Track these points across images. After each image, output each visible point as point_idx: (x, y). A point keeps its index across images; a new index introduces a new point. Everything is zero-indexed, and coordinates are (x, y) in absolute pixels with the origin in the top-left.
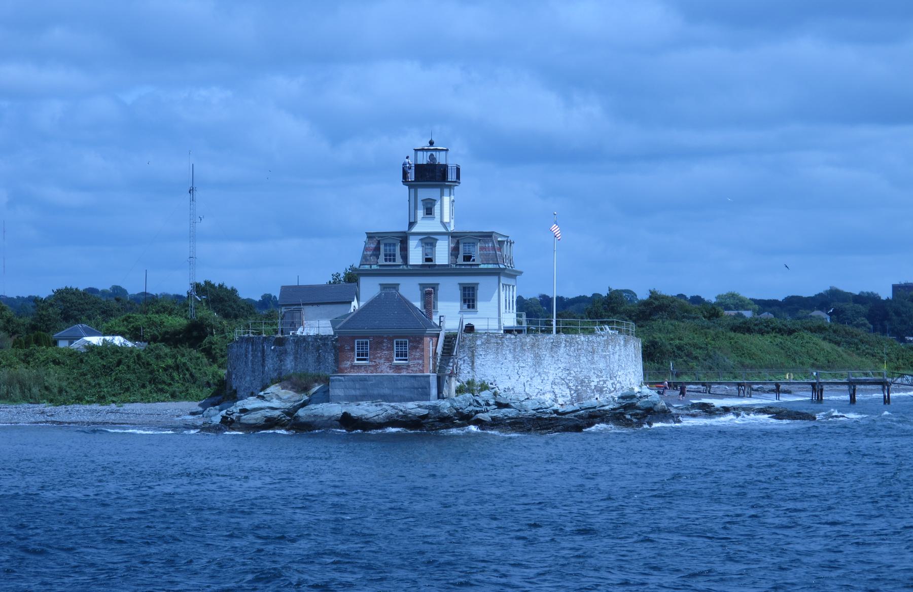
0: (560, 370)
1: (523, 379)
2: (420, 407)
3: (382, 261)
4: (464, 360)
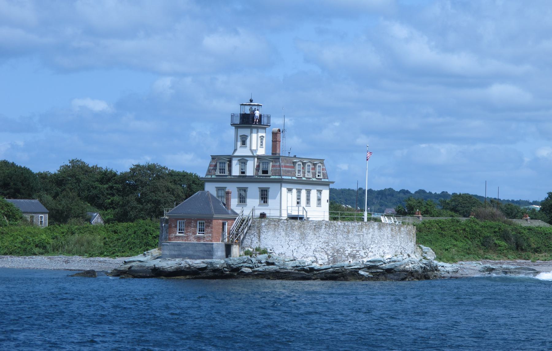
0: (321, 243)
1: (291, 248)
2: (203, 262)
3: (218, 173)
4: (254, 235)
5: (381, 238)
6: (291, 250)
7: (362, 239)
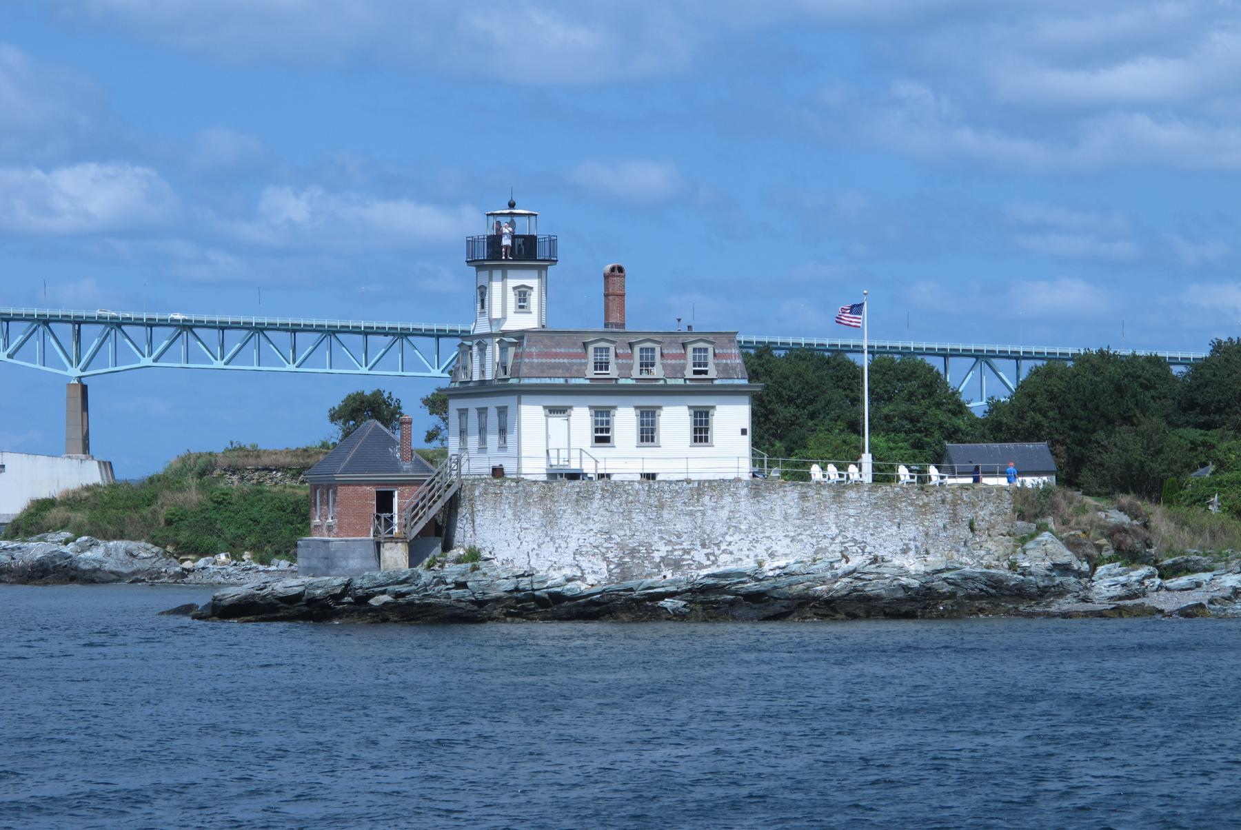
0: (592, 533)
1: (526, 547)
5: (761, 518)
7: (699, 521)
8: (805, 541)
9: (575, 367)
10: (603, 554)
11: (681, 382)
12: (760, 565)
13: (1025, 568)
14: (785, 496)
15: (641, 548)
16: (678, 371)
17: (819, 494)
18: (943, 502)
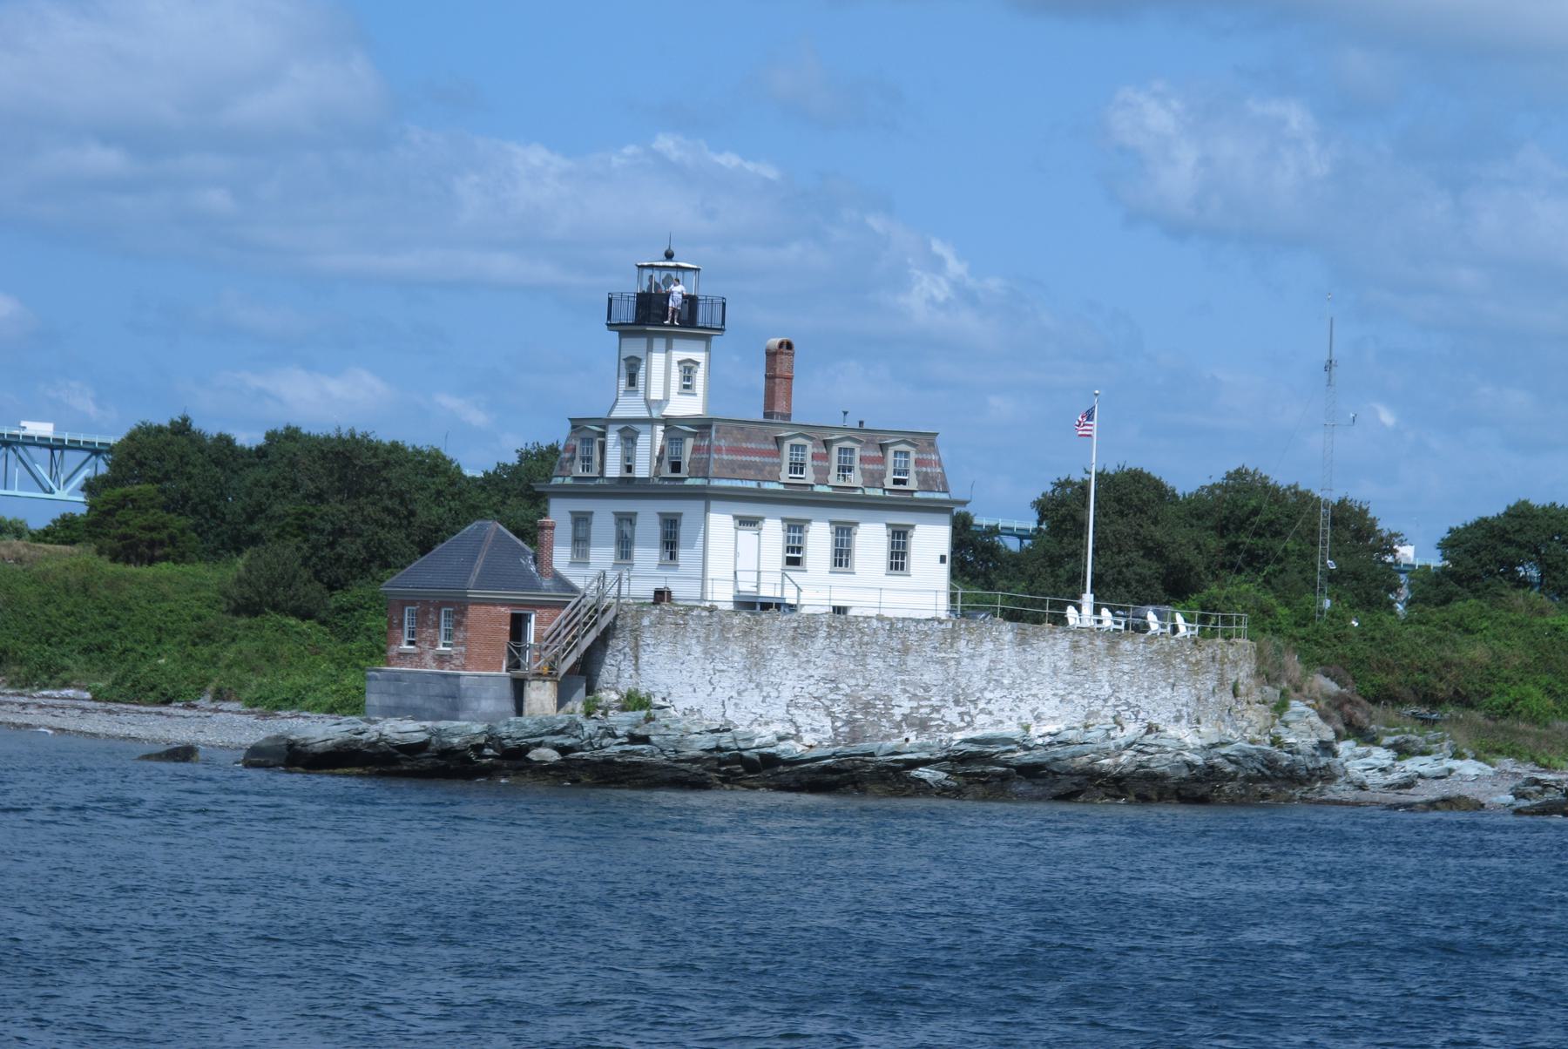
0: (812, 681)
1: (720, 694)
5: (1026, 671)
6: (720, 701)
7: (952, 671)
8: (1076, 702)
9: (768, 468)
10: (827, 708)
11: (879, 492)
12: (1027, 728)
13: (1290, 745)
14: (1054, 645)
15: (878, 702)
16: (875, 479)
17: (1092, 644)
18: (1213, 658)
